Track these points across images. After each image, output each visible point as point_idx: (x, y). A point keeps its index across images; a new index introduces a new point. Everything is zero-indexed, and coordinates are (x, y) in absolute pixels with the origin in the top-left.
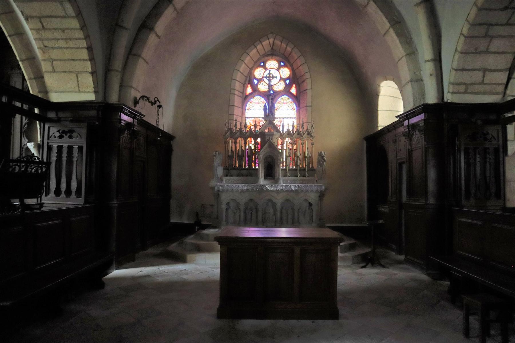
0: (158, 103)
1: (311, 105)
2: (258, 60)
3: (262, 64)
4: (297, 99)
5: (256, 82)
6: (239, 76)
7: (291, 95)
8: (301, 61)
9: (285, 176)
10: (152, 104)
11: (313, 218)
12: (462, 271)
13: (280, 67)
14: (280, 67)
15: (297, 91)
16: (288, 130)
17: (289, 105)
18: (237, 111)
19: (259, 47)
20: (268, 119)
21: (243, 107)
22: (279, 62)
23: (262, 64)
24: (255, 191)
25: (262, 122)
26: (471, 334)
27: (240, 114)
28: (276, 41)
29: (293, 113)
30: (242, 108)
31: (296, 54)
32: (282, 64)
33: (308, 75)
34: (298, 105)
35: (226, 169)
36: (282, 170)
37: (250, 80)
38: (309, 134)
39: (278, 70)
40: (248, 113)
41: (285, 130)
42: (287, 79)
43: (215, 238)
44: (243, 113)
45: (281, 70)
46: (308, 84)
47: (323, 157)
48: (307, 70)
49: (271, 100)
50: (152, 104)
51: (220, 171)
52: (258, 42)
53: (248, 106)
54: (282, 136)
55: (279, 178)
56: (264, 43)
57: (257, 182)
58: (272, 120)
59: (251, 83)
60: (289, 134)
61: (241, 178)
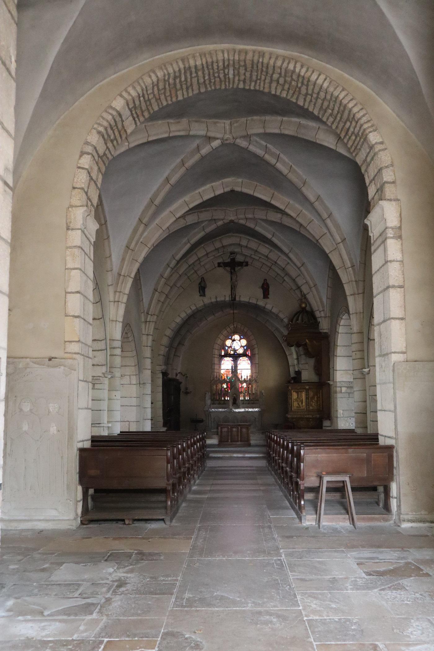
0: (186, 376)
1: (258, 363)
3: (230, 337)
4: (251, 358)
5: (227, 348)
6: (216, 346)
9: (243, 403)
10: (183, 376)
12: (242, 410)
13: (241, 339)
14: (241, 339)
16: (245, 379)
17: (247, 361)
18: (216, 367)
19: (228, 329)
20: (233, 373)
21: (220, 364)
23: (230, 337)
24: (93, 126)
25: (230, 376)
29: (249, 366)
30: (219, 364)
31: (249, 333)
32: (242, 337)
33: (256, 346)
34: (252, 363)
35: (212, 400)
37: (223, 346)
38: (256, 381)
39: (240, 341)
40: (223, 367)
41: (243, 379)
42: (245, 346)
44: (220, 367)
45: (241, 340)
46: (256, 351)
51: (209, 402)
53: (222, 362)
54: (242, 382)
58: (236, 374)
59: (224, 349)
60: (245, 381)
61: (398, 119)
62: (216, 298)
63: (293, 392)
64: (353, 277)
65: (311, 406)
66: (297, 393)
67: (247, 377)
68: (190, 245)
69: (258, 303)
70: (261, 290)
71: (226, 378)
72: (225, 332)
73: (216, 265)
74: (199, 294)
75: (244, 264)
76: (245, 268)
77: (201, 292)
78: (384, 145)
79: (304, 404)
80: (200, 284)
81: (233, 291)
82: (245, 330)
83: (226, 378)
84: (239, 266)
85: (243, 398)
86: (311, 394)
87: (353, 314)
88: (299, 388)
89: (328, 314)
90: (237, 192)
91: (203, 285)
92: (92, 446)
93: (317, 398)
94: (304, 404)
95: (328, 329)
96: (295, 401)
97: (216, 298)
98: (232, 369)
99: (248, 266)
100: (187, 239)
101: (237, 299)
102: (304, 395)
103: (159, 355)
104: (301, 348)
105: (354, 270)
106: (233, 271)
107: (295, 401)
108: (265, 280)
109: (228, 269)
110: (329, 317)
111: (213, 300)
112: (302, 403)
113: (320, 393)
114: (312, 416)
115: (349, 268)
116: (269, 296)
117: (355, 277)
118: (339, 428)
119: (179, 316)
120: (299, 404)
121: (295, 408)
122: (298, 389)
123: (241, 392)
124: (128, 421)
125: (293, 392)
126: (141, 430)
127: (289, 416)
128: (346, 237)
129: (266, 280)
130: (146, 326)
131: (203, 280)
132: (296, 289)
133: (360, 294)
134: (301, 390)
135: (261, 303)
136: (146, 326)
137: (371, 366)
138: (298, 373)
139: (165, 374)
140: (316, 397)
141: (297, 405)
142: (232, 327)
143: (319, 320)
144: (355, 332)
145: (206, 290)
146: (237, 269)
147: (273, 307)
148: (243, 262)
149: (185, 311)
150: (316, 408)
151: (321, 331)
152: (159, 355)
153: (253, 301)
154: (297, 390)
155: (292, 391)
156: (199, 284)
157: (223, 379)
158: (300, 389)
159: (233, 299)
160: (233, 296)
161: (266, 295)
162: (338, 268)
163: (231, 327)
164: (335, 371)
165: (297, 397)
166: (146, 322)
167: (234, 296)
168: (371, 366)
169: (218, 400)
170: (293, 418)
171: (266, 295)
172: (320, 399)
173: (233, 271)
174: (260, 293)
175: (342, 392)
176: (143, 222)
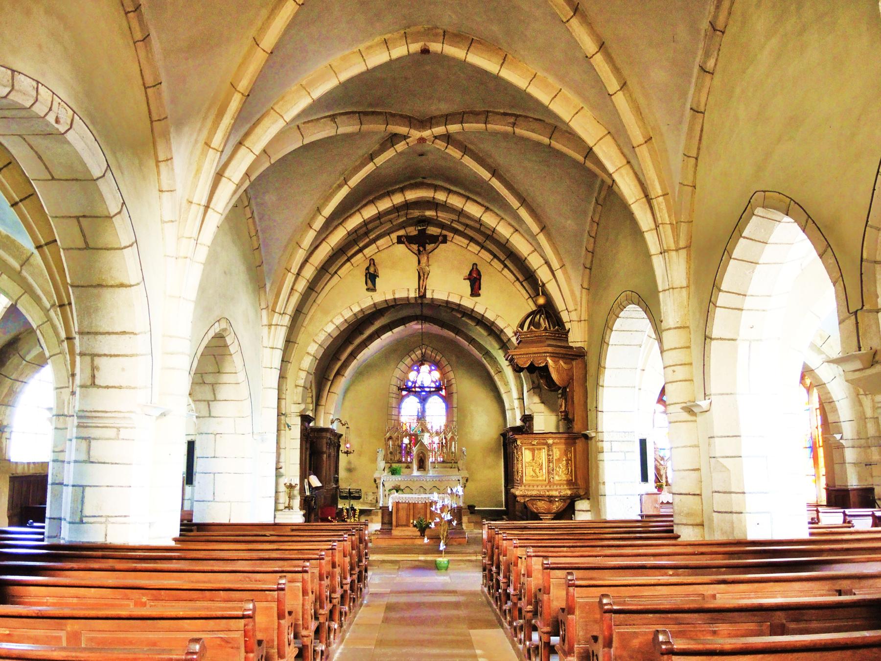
0: (347, 426)
2: (412, 365)
7: (441, 396)
8: (448, 368)
10: (343, 425)
11: (672, 240)
15: (446, 393)
19: (413, 356)
20: (420, 422)
22: (430, 366)
26: (81, 429)
27: (397, 413)
28: (427, 351)
31: (444, 362)
36: (431, 463)
43: (8, 236)
47: (463, 452)
48: (453, 377)
49: (422, 30)
50: (343, 425)
52: (412, 352)
55: (429, 470)
56: (417, 353)
57: (412, 473)
62: (394, 293)
63: (525, 449)
64: (666, 215)
65: (556, 474)
66: (533, 451)
67: (441, 427)
68: (348, 188)
69: (463, 303)
70: (468, 282)
71: (408, 428)
72: (408, 361)
73: (395, 241)
74: (366, 287)
75: (440, 238)
76: (442, 246)
77: (369, 282)
78: (308, 631)
79: (544, 472)
80: (368, 269)
81: (421, 281)
82: (438, 358)
83: (408, 428)
84: (432, 243)
85: (434, 459)
86: (557, 453)
87: (665, 290)
88: (535, 442)
89: (584, 316)
90: (436, 53)
91: (372, 270)
92: (181, 535)
93: (566, 460)
94: (544, 472)
95: (585, 341)
96: (527, 465)
97: (394, 293)
98: (418, 416)
99: (446, 243)
100: (343, 178)
101: (429, 295)
102: (543, 454)
103: (296, 386)
104: (535, 375)
105: (667, 202)
106: (421, 249)
107: (527, 465)
108: (475, 264)
109: (415, 247)
110: (585, 320)
111: (389, 297)
112: (541, 469)
113: (571, 452)
114: (560, 492)
115: (659, 197)
116: (480, 292)
117: (669, 216)
118: (609, 517)
119: (331, 321)
120: (534, 471)
121: (529, 478)
122: (534, 445)
123: (432, 451)
124: (229, 502)
125: (525, 449)
126: (226, 521)
127: (517, 493)
128: (651, 135)
129: (476, 264)
130: (269, 333)
131: (372, 262)
132: (524, 281)
133: (680, 249)
134: (539, 447)
135: (468, 302)
136: (269, 333)
137: (715, 395)
138: (528, 419)
139: (305, 419)
140: (564, 459)
141: (532, 473)
142: (419, 352)
143: (567, 326)
144: (672, 326)
145: (377, 280)
146: (429, 247)
147: (487, 308)
148: (439, 236)
149: (341, 314)
150: (566, 479)
151: (571, 344)
152: (296, 386)
153: (454, 299)
154: (531, 447)
155: (523, 448)
156: (366, 270)
157: (404, 429)
158: (538, 444)
159: (421, 294)
160: (421, 289)
161: (475, 291)
162: (634, 200)
163: (417, 353)
164: (599, 414)
165: (531, 458)
166: (270, 325)
167: (423, 291)
168: (715, 395)
169: (404, 463)
170: (524, 496)
171: (475, 291)
172: (572, 462)
173: (421, 249)
174: (466, 286)
175: (613, 450)
176: (238, 89)
